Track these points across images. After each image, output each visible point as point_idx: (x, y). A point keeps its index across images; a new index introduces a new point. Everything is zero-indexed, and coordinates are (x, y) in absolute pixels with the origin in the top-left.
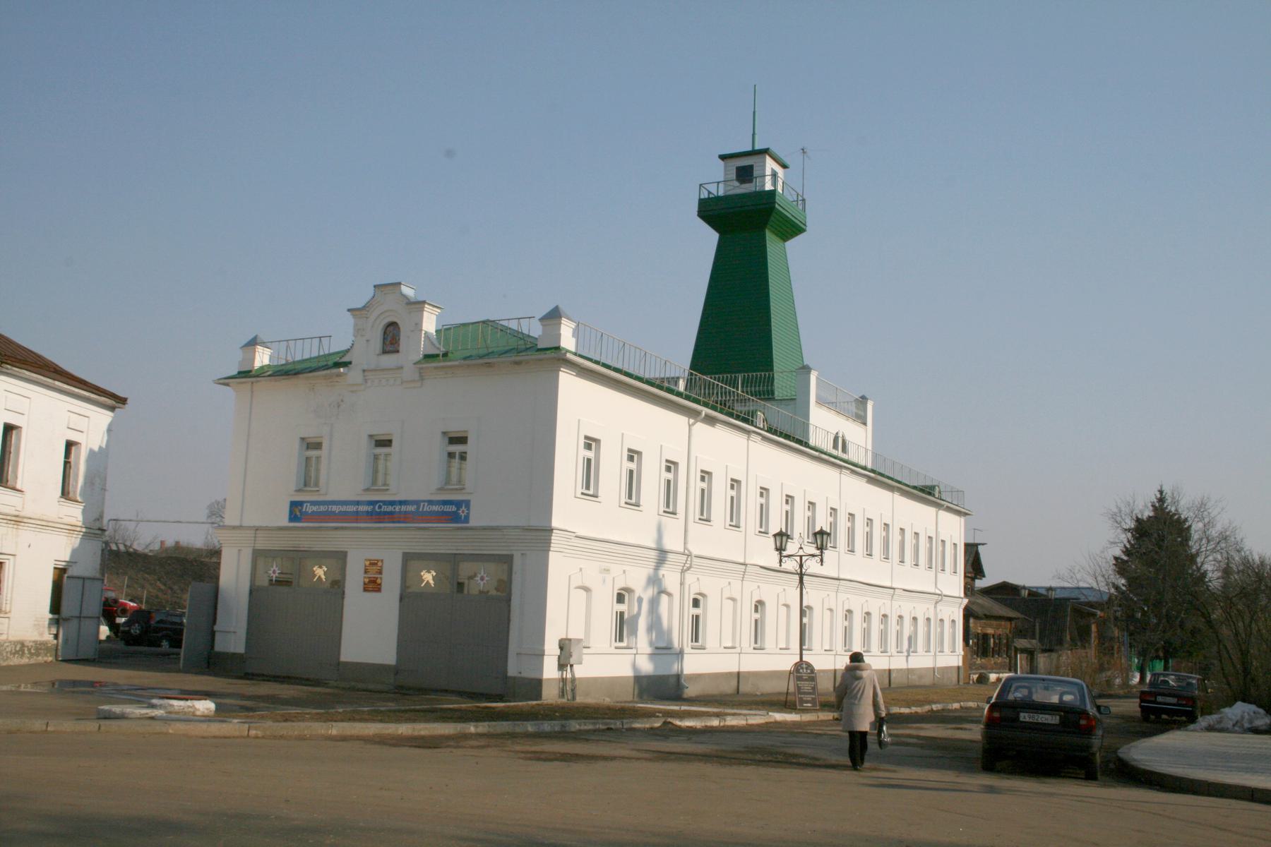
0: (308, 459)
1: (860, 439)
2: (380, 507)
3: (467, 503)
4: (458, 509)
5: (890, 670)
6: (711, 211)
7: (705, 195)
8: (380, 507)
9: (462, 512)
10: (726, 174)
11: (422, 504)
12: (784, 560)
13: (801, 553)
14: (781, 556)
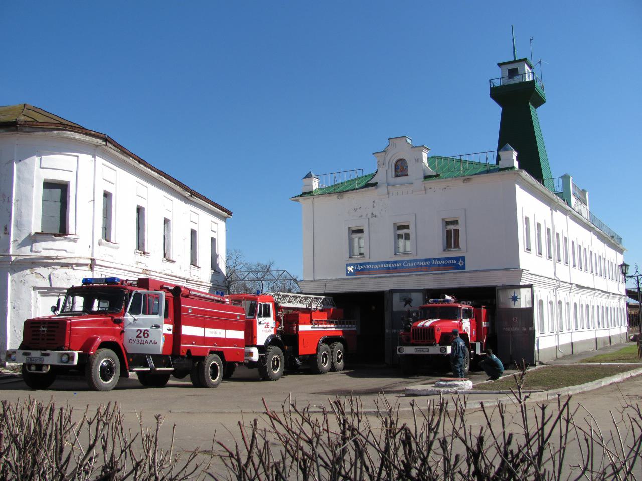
0: (448, 233)
1: (584, 211)
2: (406, 264)
3: (463, 258)
4: (458, 261)
5: (610, 337)
6: (497, 94)
7: (492, 86)
8: (406, 264)
9: (461, 263)
10: (502, 74)
11: (433, 260)
12: (627, 279)
13: (637, 274)
14: (625, 277)
